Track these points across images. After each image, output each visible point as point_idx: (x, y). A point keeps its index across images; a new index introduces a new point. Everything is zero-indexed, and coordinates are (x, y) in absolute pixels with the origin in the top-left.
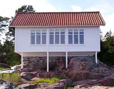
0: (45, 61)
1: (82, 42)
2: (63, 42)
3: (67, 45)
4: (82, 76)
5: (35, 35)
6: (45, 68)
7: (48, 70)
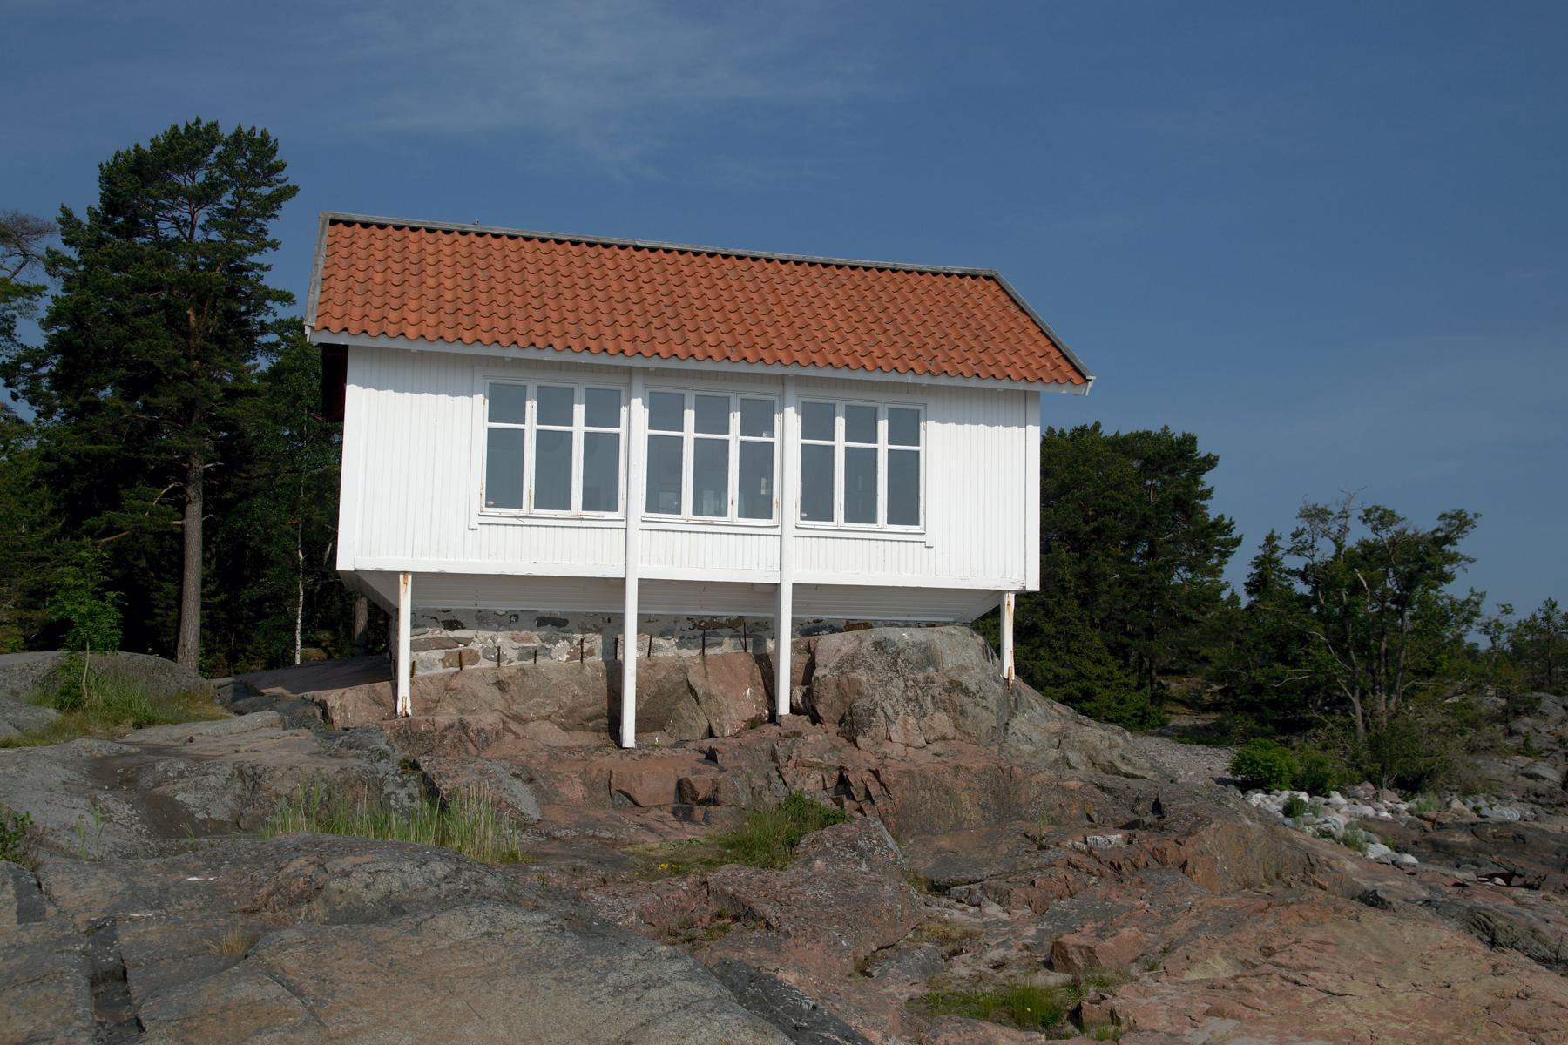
1: (906, 509)
4: (965, 797)
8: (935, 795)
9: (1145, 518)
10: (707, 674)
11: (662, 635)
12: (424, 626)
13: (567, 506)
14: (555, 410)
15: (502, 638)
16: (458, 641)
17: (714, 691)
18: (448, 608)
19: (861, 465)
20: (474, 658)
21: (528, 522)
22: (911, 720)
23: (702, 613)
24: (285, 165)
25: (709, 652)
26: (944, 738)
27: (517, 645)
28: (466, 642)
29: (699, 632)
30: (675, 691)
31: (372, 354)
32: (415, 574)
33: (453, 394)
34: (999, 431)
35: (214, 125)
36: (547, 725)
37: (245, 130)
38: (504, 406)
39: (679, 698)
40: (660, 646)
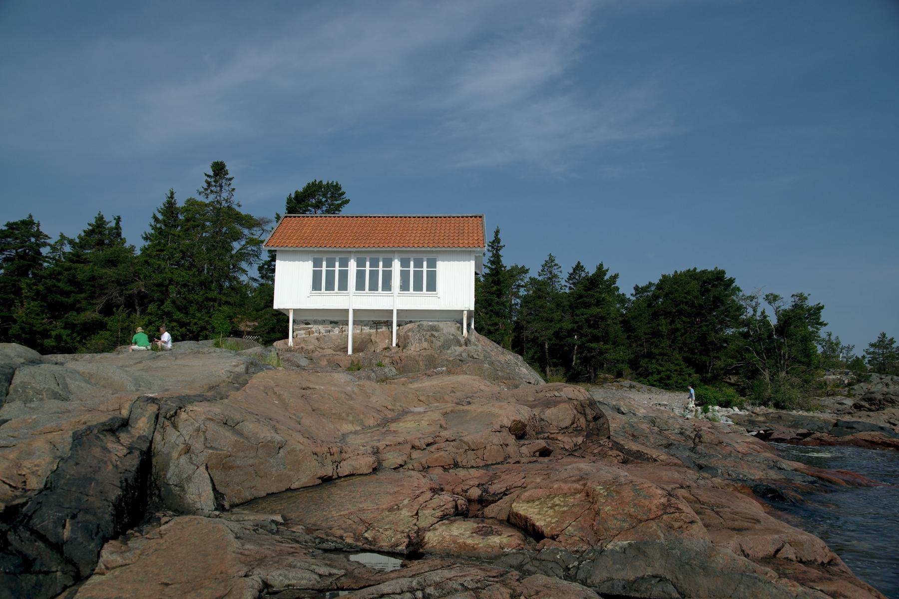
0: (345, 331)
1: (432, 287)
2: (343, 286)
3: (351, 294)
4: (421, 363)
5: (339, 267)
6: (345, 348)
7: (350, 352)
9: (700, 305)
11: (365, 326)
13: (334, 290)
14: (331, 264)
15: (320, 327)
16: (309, 328)
17: (377, 341)
20: (313, 332)
22: (418, 344)
24: (345, 193)
26: (425, 349)
28: (311, 328)
29: (375, 325)
31: (282, 251)
32: (294, 310)
33: (284, 261)
34: (462, 263)
35: (321, 182)
36: (330, 350)
37: (330, 182)
38: (317, 263)
39: (368, 343)
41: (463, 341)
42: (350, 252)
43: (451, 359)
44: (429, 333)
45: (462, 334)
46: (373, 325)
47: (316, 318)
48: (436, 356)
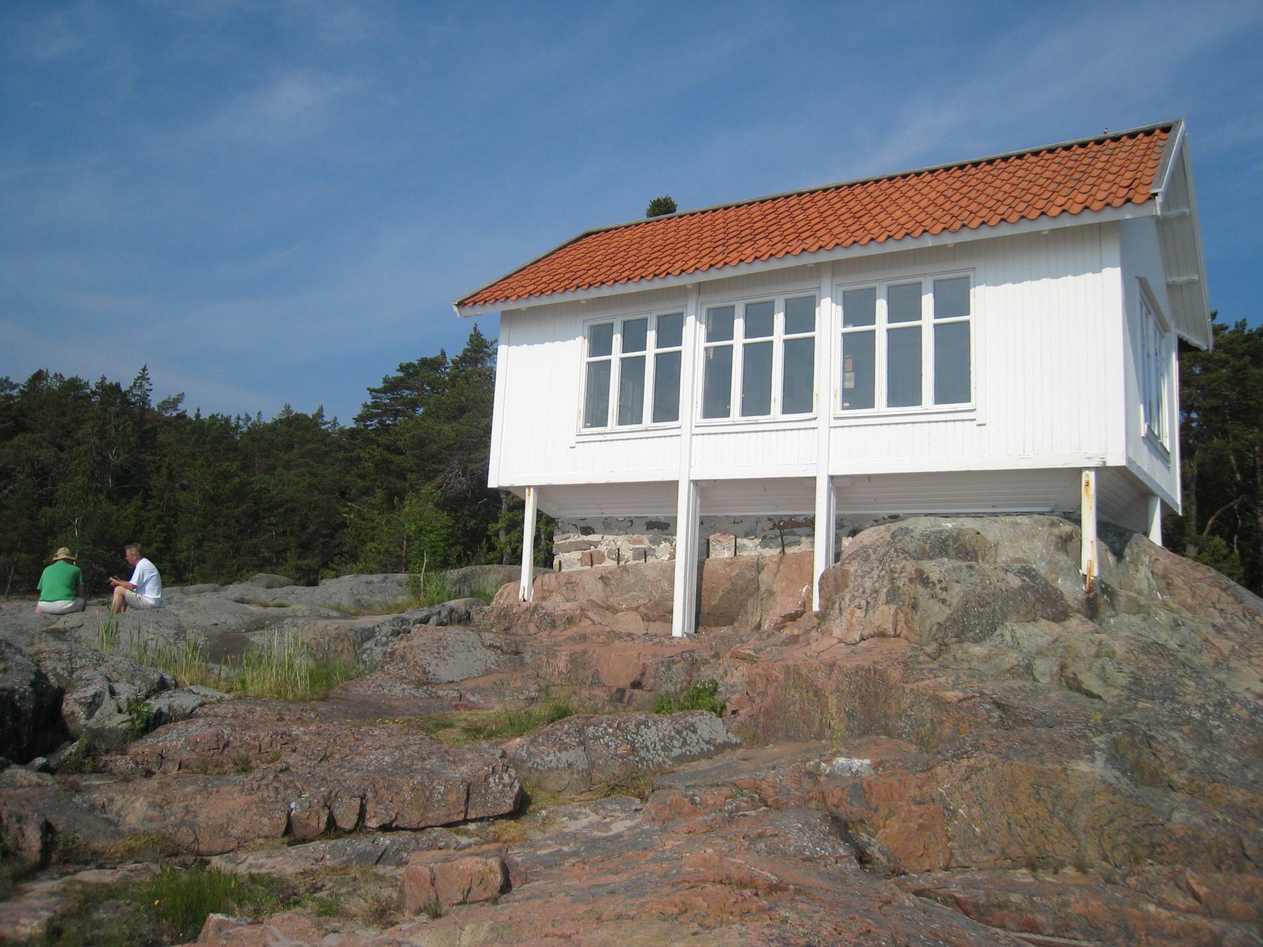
2: (667, 409)
3: (685, 431)
4: (832, 701)
7: (680, 624)
8: (805, 695)
10: (778, 571)
11: (746, 535)
12: (568, 532)
16: (591, 544)
17: (775, 588)
18: (584, 516)
19: (758, 358)
20: (601, 558)
21: (609, 437)
23: (761, 514)
25: (789, 551)
27: (631, 546)
28: (596, 544)
29: (777, 532)
30: (747, 588)
36: (632, 615)
38: (599, 343)
40: (744, 545)
41: (1072, 591)
42: (682, 292)
43: (953, 695)
44: (910, 566)
45: (1079, 565)
46: (771, 534)
47: (609, 513)
48: (895, 674)
